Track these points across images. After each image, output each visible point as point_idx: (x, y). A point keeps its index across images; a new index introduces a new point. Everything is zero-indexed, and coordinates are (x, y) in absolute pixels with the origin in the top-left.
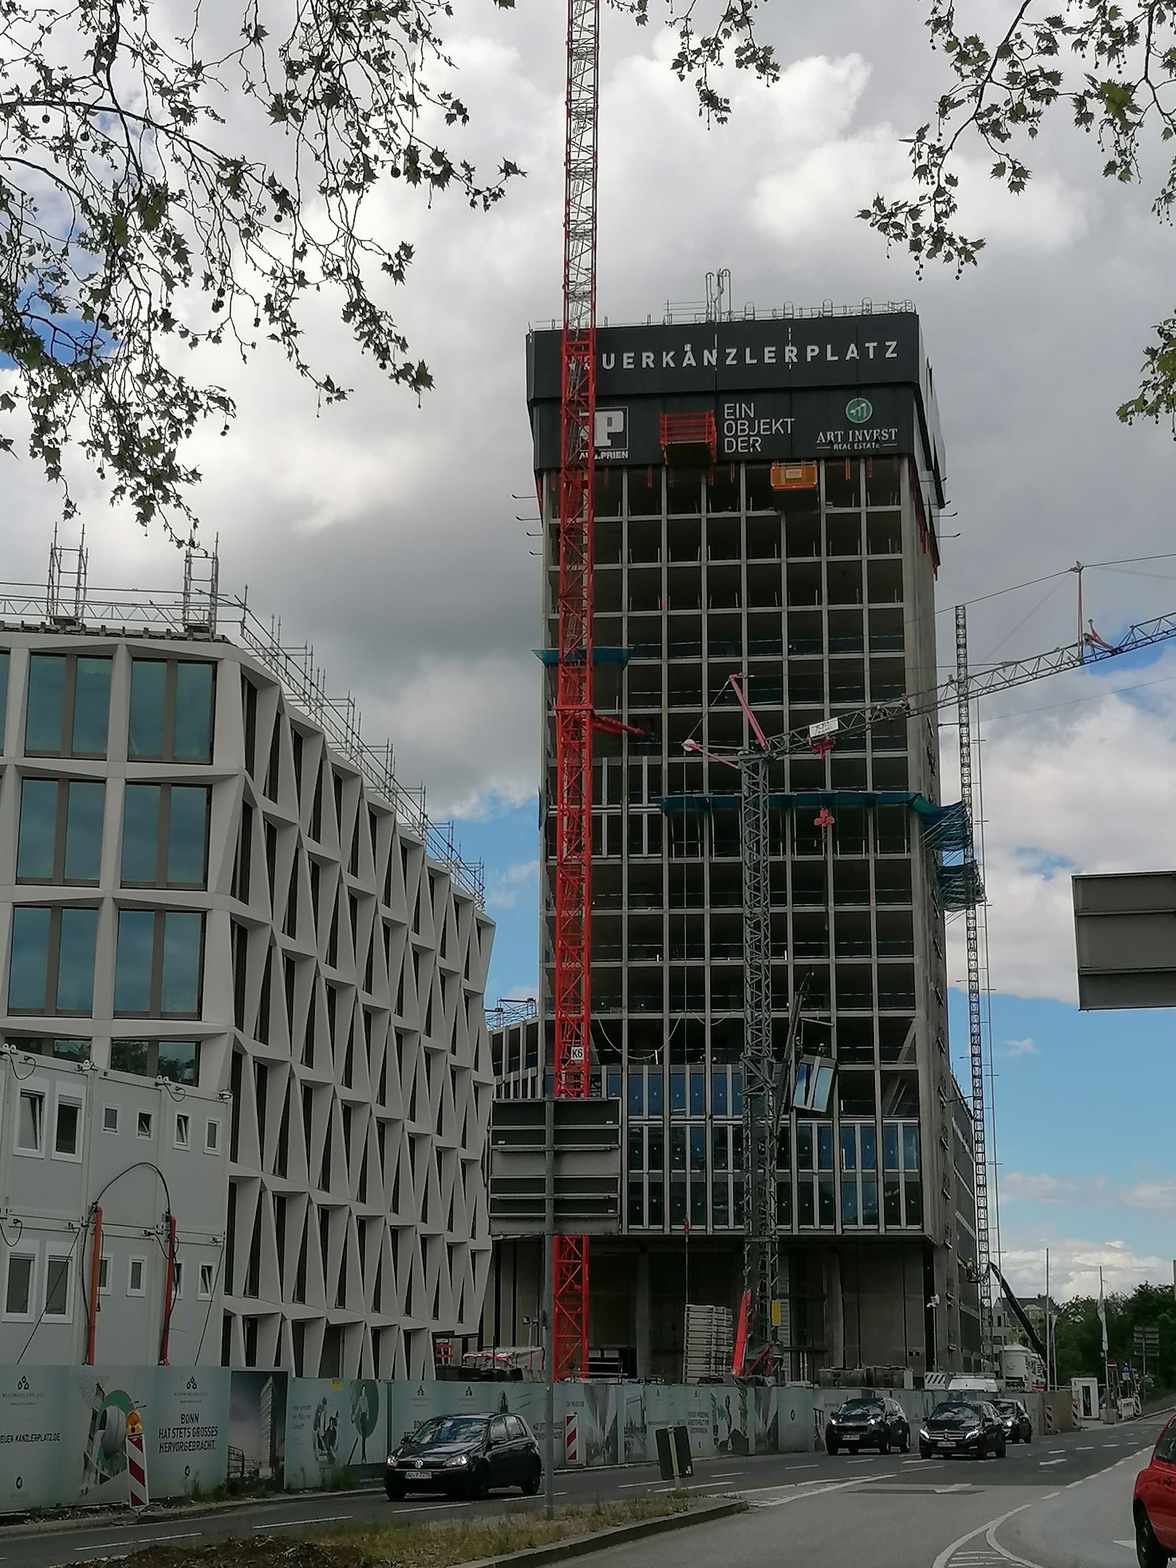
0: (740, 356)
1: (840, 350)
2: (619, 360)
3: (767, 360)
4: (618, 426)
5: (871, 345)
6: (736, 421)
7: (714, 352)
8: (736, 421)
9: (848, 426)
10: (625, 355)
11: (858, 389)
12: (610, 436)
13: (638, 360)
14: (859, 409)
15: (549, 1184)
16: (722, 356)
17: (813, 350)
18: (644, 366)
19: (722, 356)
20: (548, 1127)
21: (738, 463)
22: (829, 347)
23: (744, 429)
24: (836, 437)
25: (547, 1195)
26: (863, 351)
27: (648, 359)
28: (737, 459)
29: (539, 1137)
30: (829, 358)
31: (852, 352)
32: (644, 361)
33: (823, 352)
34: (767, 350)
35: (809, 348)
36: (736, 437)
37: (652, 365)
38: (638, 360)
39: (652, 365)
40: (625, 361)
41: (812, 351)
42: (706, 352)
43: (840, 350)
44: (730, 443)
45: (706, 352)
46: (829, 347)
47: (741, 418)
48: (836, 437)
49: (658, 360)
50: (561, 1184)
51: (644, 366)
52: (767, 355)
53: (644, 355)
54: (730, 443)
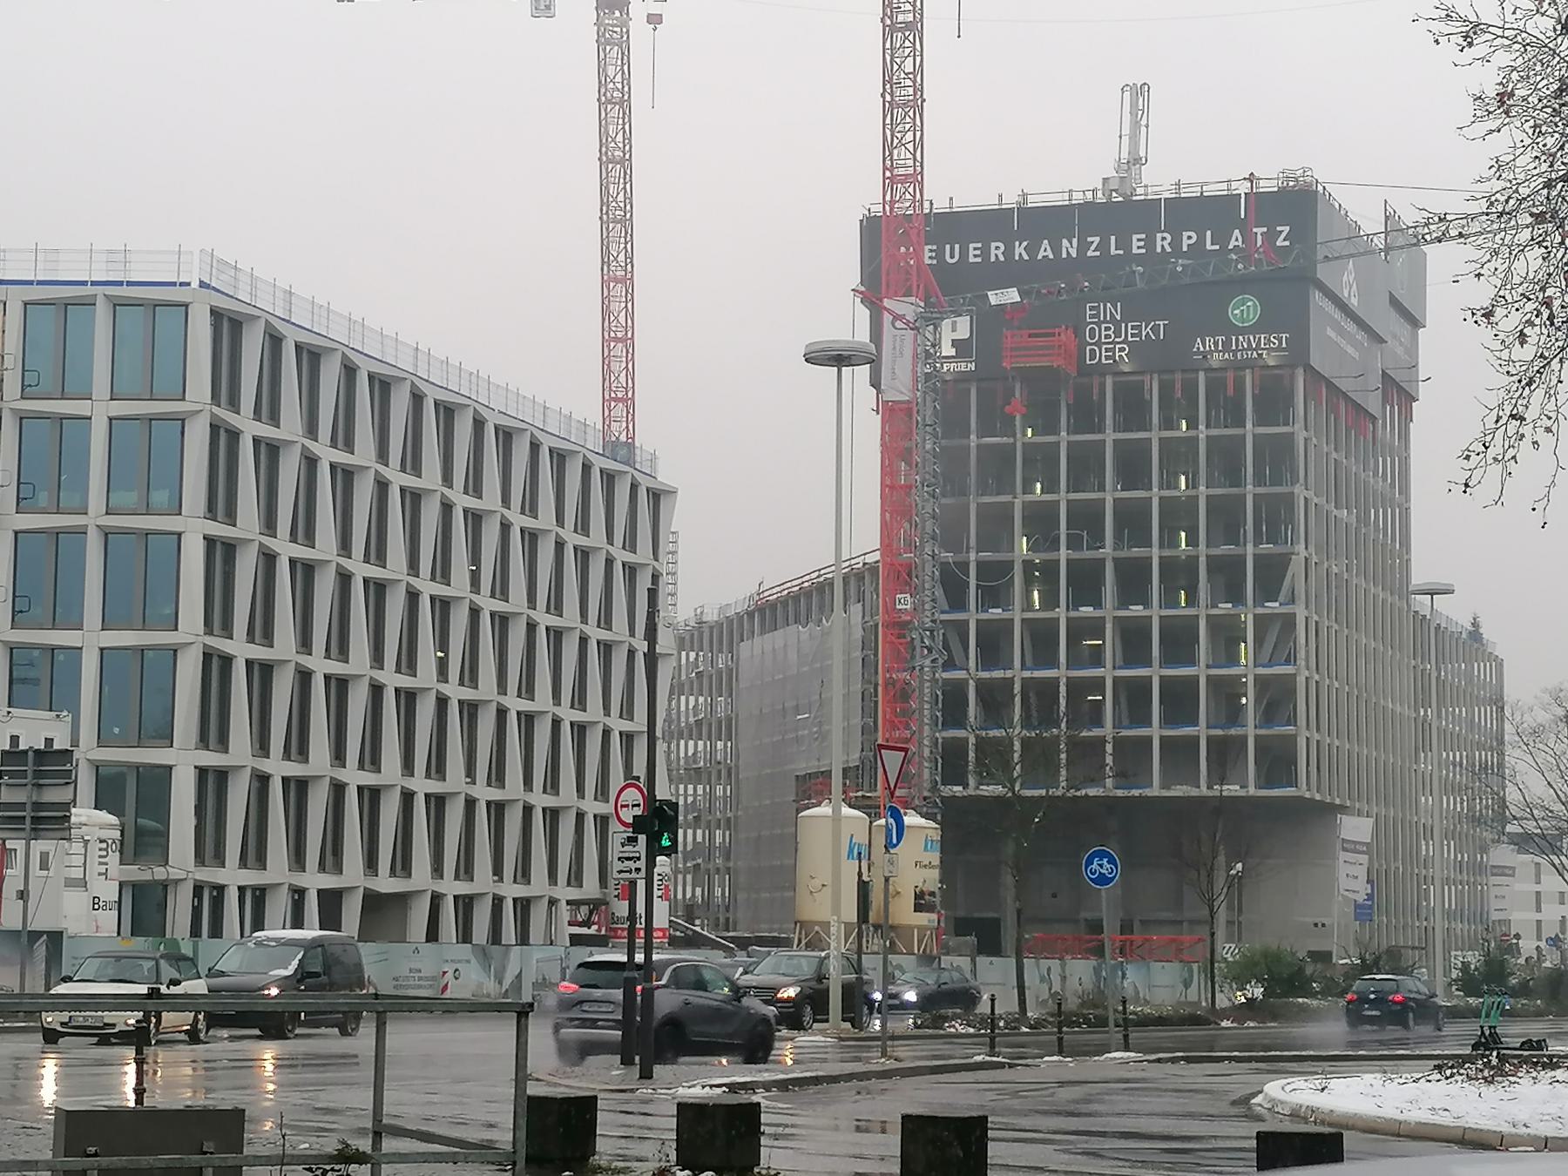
0: (1103, 246)
1: (1222, 238)
2: (964, 253)
3: (1135, 251)
4: (963, 332)
5: (1259, 230)
6: (1098, 324)
7: (1075, 241)
8: (1098, 324)
9: (1231, 330)
10: (972, 246)
11: (1244, 284)
12: (955, 343)
13: (985, 252)
14: (1245, 310)
15: (28, 807)
16: (1083, 246)
17: (1164, 239)
18: (1159, 250)
19: (1083, 246)
20: (30, 768)
21: (1103, 375)
22: (1209, 233)
23: (1112, 341)
24: (1216, 344)
25: (28, 813)
26: (1248, 237)
27: (997, 250)
28: (1101, 370)
29: (23, 774)
30: (1209, 247)
31: (1045, 251)
32: (1159, 243)
33: (1201, 239)
34: (1135, 237)
35: (1186, 234)
36: (1099, 344)
37: (1169, 250)
38: (985, 252)
39: (1169, 250)
40: (971, 252)
41: (1188, 238)
42: (1065, 242)
43: (1222, 238)
44: (1093, 351)
45: (1065, 242)
46: (1209, 233)
47: (1105, 321)
48: (1216, 344)
49: (1009, 252)
50: (38, 806)
51: (1159, 250)
52: (1135, 244)
53: (994, 245)
54: (1093, 351)
